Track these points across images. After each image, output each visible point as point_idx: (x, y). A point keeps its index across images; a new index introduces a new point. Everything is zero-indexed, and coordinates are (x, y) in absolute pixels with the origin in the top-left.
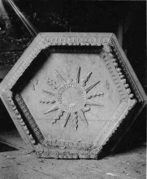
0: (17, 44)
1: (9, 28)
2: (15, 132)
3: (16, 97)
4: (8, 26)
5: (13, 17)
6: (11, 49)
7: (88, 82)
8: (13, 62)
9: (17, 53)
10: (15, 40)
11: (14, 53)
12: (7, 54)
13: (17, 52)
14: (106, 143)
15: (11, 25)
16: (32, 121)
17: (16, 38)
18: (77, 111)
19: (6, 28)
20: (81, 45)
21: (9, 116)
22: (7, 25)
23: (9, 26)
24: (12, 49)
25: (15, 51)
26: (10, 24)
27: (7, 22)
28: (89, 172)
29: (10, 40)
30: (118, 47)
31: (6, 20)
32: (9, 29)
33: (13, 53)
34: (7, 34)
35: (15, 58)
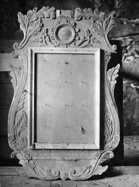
0: (132, 26)
1: (120, 7)
3: (105, 56)
4: (119, 5)
6: (124, 33)
8: (127, 50)
9: (133, 38)
10: (129, 21)
11: (127, 38)
13: (133, 37)
15: (123, 3)
16: (63, 18)
17: (130, 19)
18: (68, 146)
19: (116, 8)
22: (117, 4)
24: (125, 33)
28: (65, 164)
29: (122, 23)
30: (117, 124)
33: (126, 38)
35: (131, 44)
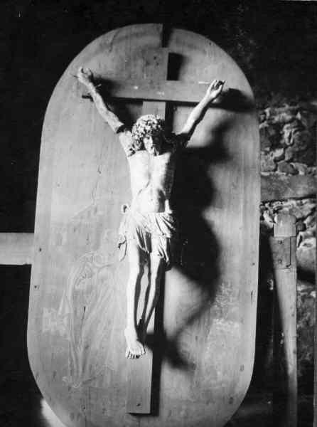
2: (268, 149)
5: (301, 114)
7: (253, 252)
11: (306, 203)
12: (287, 207)
14: (210, 137)
15: (298, 133)
20: (120, 124)
21: (47, 105)
22: (286, 135)
23: (293, 136)
24: (300, 193)
25: (304, 311)
26: (295, 132)
27: (288, 128)
29: (296, 172)
31: (285, 123)
32: (292, 145)
33: (304, 201)
34: (287, 159)
